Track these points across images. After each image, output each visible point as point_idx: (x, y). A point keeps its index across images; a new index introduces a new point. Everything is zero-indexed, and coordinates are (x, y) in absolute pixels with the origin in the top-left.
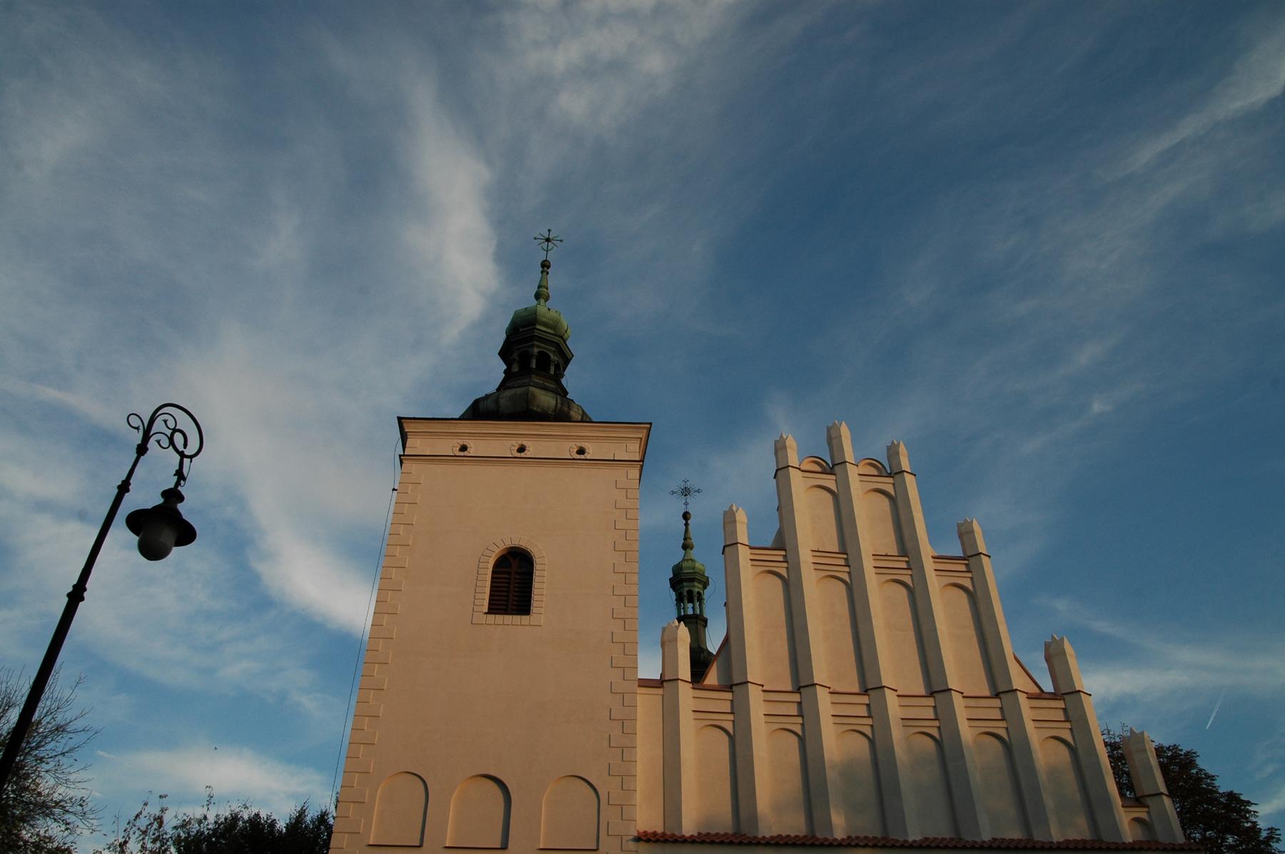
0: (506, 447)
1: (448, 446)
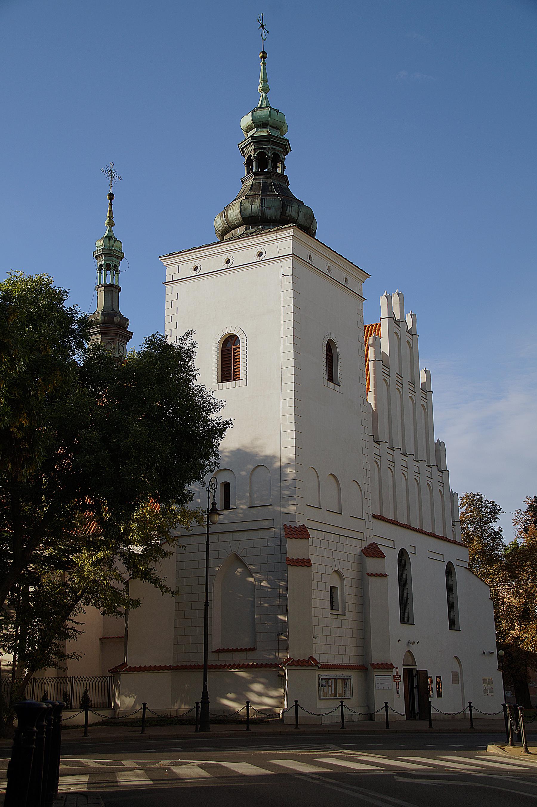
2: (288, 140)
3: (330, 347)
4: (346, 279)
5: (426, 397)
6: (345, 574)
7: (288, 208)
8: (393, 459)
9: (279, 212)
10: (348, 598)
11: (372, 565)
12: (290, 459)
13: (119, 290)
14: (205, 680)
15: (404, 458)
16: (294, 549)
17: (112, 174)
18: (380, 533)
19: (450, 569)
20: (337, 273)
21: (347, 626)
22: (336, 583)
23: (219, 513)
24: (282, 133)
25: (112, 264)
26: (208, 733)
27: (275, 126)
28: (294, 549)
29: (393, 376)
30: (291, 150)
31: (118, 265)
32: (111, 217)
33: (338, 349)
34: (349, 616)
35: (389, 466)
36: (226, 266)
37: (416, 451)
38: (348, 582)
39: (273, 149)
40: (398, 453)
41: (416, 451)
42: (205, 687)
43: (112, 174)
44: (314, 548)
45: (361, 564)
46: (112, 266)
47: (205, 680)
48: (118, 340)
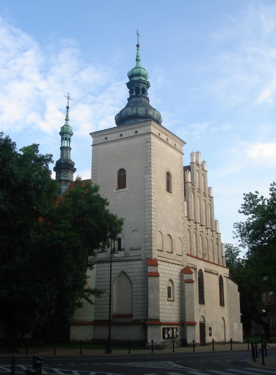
0: (131, 133)
1: (116, 136)
2: (149, 82)
3: (168, 174)
4: (167, 139)
5: (194, 188)
6: (174, 281)
7: (149, 112)
8: (218, 238)
9: (145, 113)
10: (176, 292)
11: (186, 277)
12: (108, 211)
13: (71, 149)
14: (110, 330)
15: (201, 227)
16: (151, 269)
17: (68, 98)
18: (192, 261)
19: (221, 279)
20: (163, 136)
21: (176, 304)
22: (171, 285)
23: (116, 252)
24: (146, 79)
25: (68, 137)
26: (110, 354)
27: (143, 75)
28: (151, 269)
29: (196, 189)
30: (150, 86)
31: (70, 138)
32: (67, 117)
33: (172, 177)
34: (176, 300)
35: (194, 231)
36: (120, 138)
37: (212, 227)
38: (176, 285)
39: (142, 85)
40: (198, 225)
41: (212, 227)
42: (110, 334)
43: (68, 98)
44: (162, 268)
45: (181, 276)
46: (68, 139)
47: (110, 330)
48: (70, 172)
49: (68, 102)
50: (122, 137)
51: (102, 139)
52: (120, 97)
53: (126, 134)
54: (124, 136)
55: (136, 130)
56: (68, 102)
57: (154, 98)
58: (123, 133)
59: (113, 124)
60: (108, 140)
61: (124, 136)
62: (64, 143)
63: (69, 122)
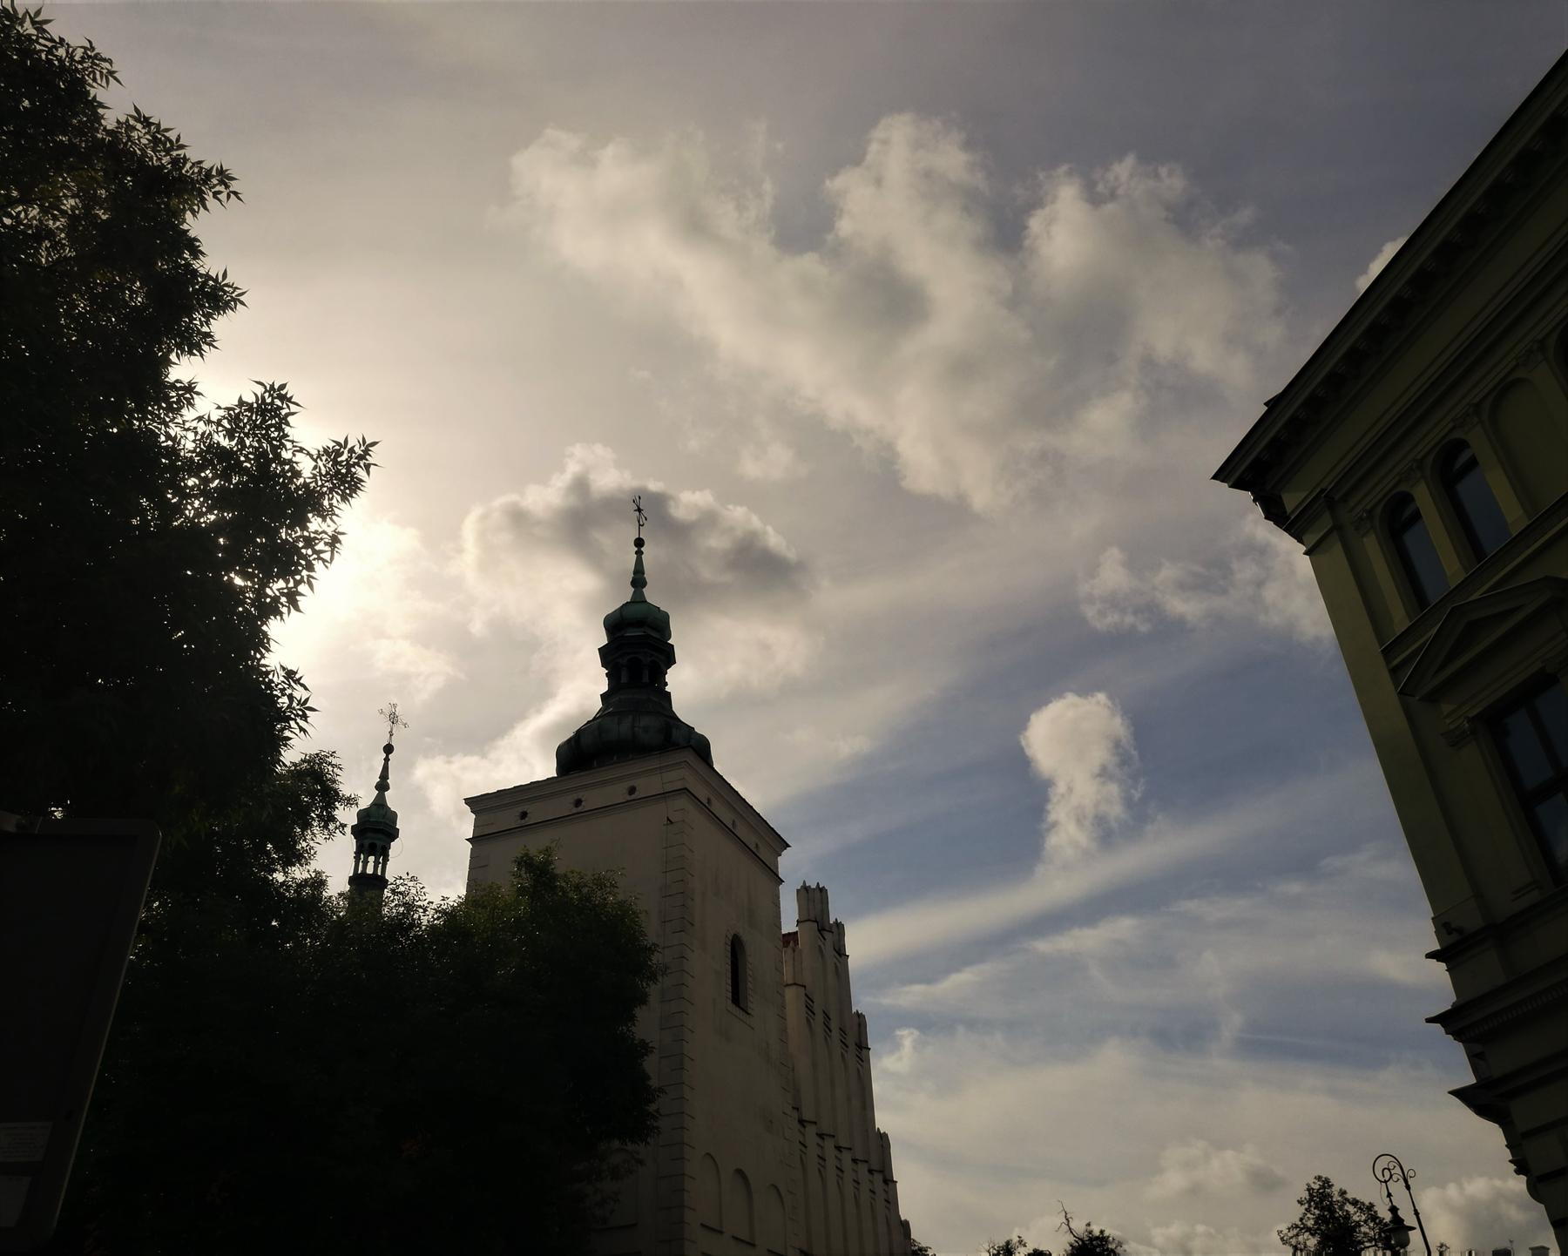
0: (617, 793)
1: (564, 806)
17: (393, 719)
36: (575, 810)
49: (384, 775)
50: (520, 809)
51: (509, 819)
52: (582, 689)
53: (593, 799)
54: (585, 806)
55: (631, 783)
56: (384, 775)
57: (685, 685)
58: (636, 783)
59: (544, 768)
60: (529, 820)
61: (585, 806)
62: (366, 863)
63: (415, 702)
